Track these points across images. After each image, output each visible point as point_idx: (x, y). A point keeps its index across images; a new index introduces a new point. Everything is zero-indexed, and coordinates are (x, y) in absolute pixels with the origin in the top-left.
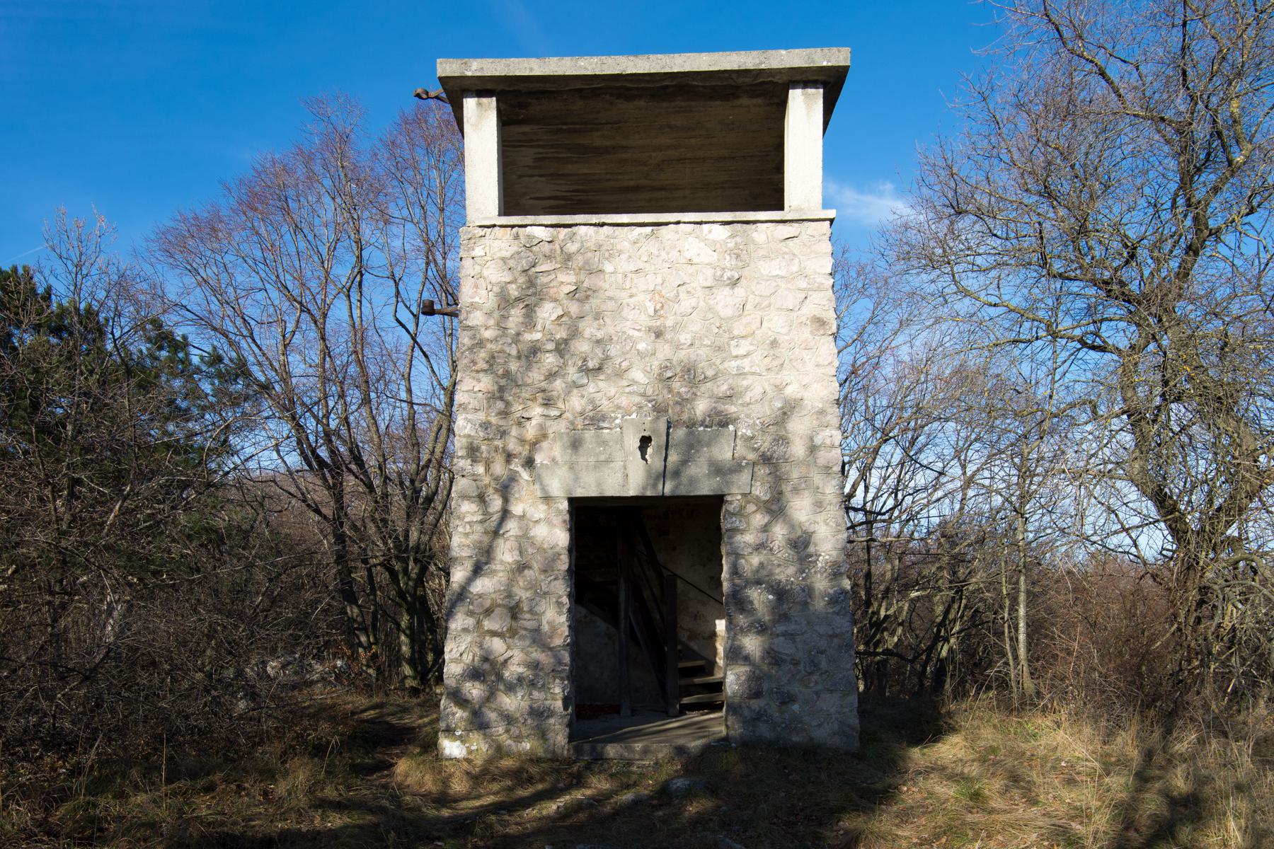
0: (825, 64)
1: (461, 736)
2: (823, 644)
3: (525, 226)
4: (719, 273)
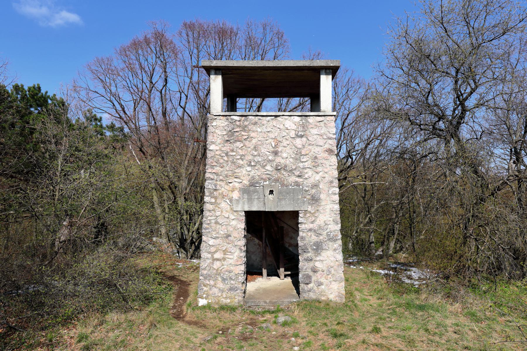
0: (332, 65)
1: (205, 297)
2: (332, 264)
3: (230, 116)
4: (297, 133)
